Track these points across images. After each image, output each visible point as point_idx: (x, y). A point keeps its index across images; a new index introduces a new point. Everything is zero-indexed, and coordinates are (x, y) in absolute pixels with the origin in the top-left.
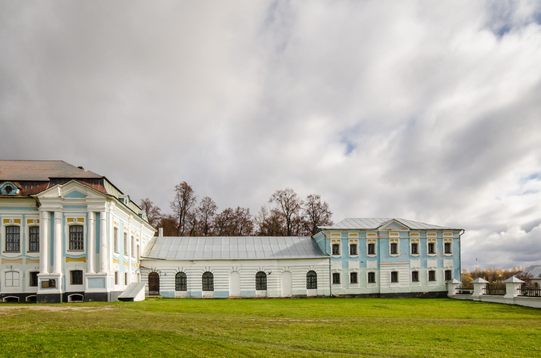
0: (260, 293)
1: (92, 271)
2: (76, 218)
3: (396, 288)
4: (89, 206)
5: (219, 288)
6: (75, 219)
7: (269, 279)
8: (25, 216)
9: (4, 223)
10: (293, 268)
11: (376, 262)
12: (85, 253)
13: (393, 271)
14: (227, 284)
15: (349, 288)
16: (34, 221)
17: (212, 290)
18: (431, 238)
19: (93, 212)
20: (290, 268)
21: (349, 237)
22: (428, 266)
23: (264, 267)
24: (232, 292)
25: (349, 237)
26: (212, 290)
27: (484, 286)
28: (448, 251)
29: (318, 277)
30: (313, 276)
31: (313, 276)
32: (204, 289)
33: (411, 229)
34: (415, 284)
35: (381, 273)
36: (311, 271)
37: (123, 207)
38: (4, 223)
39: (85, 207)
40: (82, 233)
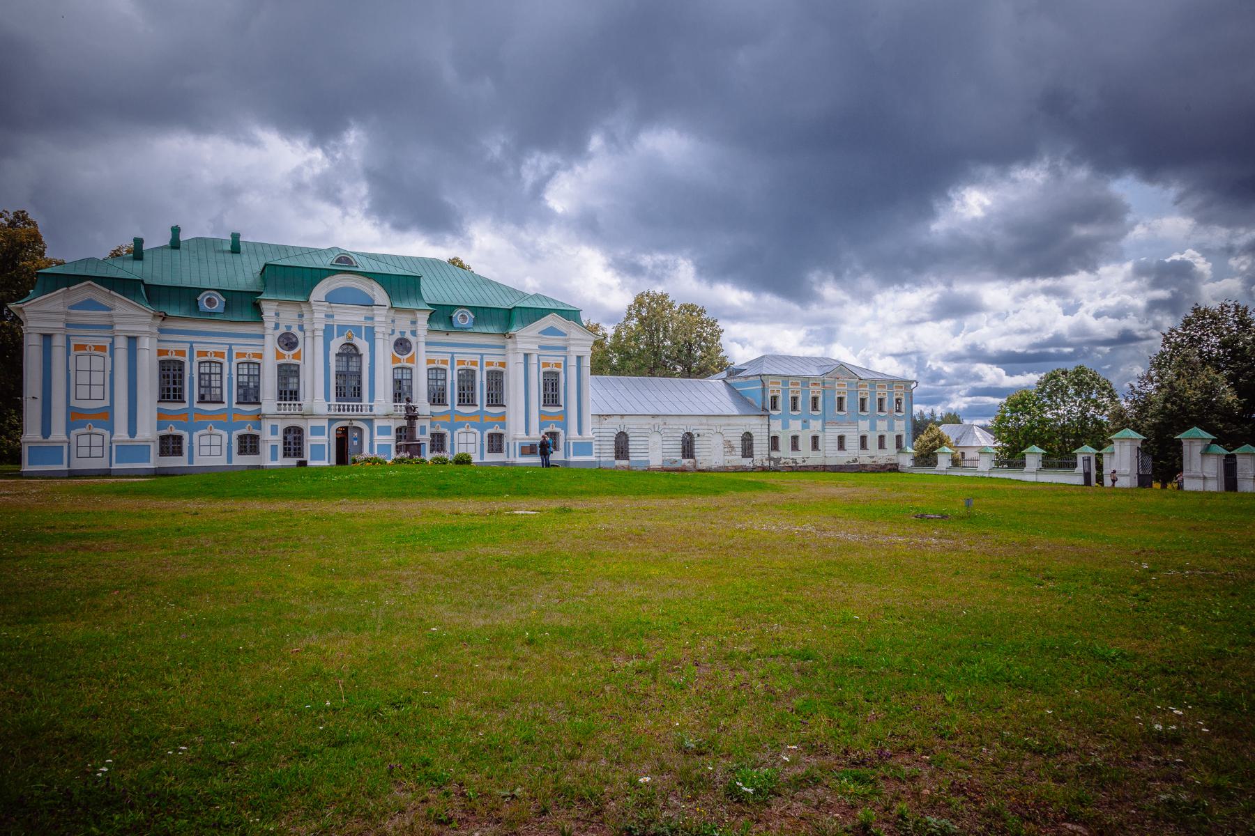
0: (686, 462)
1: (573, 432)
2: (90, 344)
3: (815, 459)
4: (117, 327)
5: (637, 454)
6: (90, 347)
7: (698, 442)
8: (71, 338)
9: (198, 357)
10: (726, 428)
11: (820, 422)
12: (108, 404)
13: (840, 434)
14: (647, 451)
15: (31, 475)
16: (87, 348)
17: (627, 458)
18: (881, 392)
19: (41, 334)
20: (723, 428)
21: (895, 390)
22: (878, 429)
23: (693, 426)
24: (656, 460)
25: (895, 390)
26: (627, 458)
27: (911, 457)
28: (815, 407)
29: (754, 442)
30: (749, 440)
31: (749, 440)
32: (684, 457)
33: (860, 379)
34: (841, 454)
35: (827, 438)
36: (748, 433)
37: (446, 341)
38: (198, 357)
39: (111, 327)
40: (359, 375)
